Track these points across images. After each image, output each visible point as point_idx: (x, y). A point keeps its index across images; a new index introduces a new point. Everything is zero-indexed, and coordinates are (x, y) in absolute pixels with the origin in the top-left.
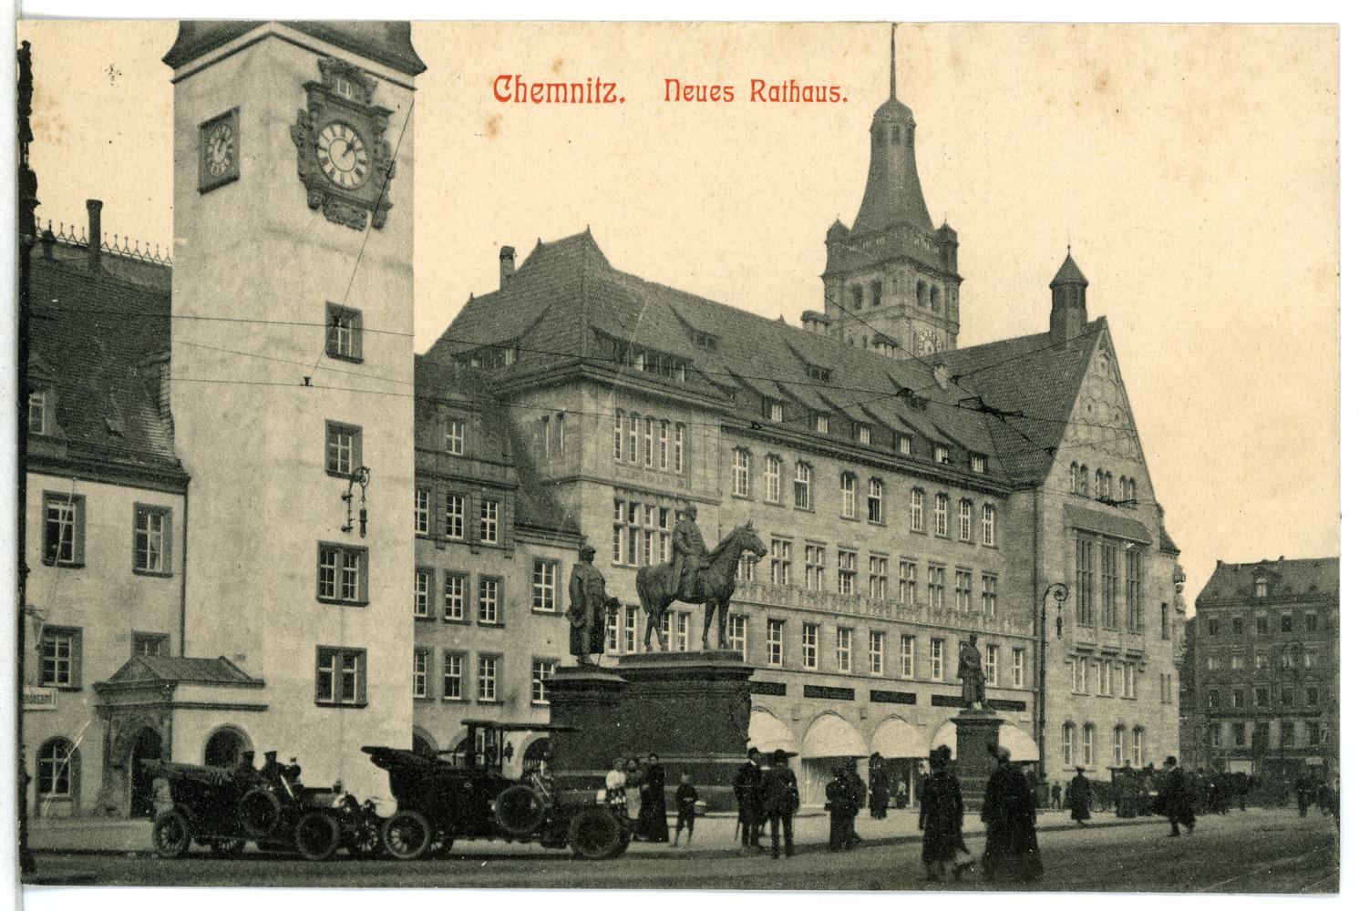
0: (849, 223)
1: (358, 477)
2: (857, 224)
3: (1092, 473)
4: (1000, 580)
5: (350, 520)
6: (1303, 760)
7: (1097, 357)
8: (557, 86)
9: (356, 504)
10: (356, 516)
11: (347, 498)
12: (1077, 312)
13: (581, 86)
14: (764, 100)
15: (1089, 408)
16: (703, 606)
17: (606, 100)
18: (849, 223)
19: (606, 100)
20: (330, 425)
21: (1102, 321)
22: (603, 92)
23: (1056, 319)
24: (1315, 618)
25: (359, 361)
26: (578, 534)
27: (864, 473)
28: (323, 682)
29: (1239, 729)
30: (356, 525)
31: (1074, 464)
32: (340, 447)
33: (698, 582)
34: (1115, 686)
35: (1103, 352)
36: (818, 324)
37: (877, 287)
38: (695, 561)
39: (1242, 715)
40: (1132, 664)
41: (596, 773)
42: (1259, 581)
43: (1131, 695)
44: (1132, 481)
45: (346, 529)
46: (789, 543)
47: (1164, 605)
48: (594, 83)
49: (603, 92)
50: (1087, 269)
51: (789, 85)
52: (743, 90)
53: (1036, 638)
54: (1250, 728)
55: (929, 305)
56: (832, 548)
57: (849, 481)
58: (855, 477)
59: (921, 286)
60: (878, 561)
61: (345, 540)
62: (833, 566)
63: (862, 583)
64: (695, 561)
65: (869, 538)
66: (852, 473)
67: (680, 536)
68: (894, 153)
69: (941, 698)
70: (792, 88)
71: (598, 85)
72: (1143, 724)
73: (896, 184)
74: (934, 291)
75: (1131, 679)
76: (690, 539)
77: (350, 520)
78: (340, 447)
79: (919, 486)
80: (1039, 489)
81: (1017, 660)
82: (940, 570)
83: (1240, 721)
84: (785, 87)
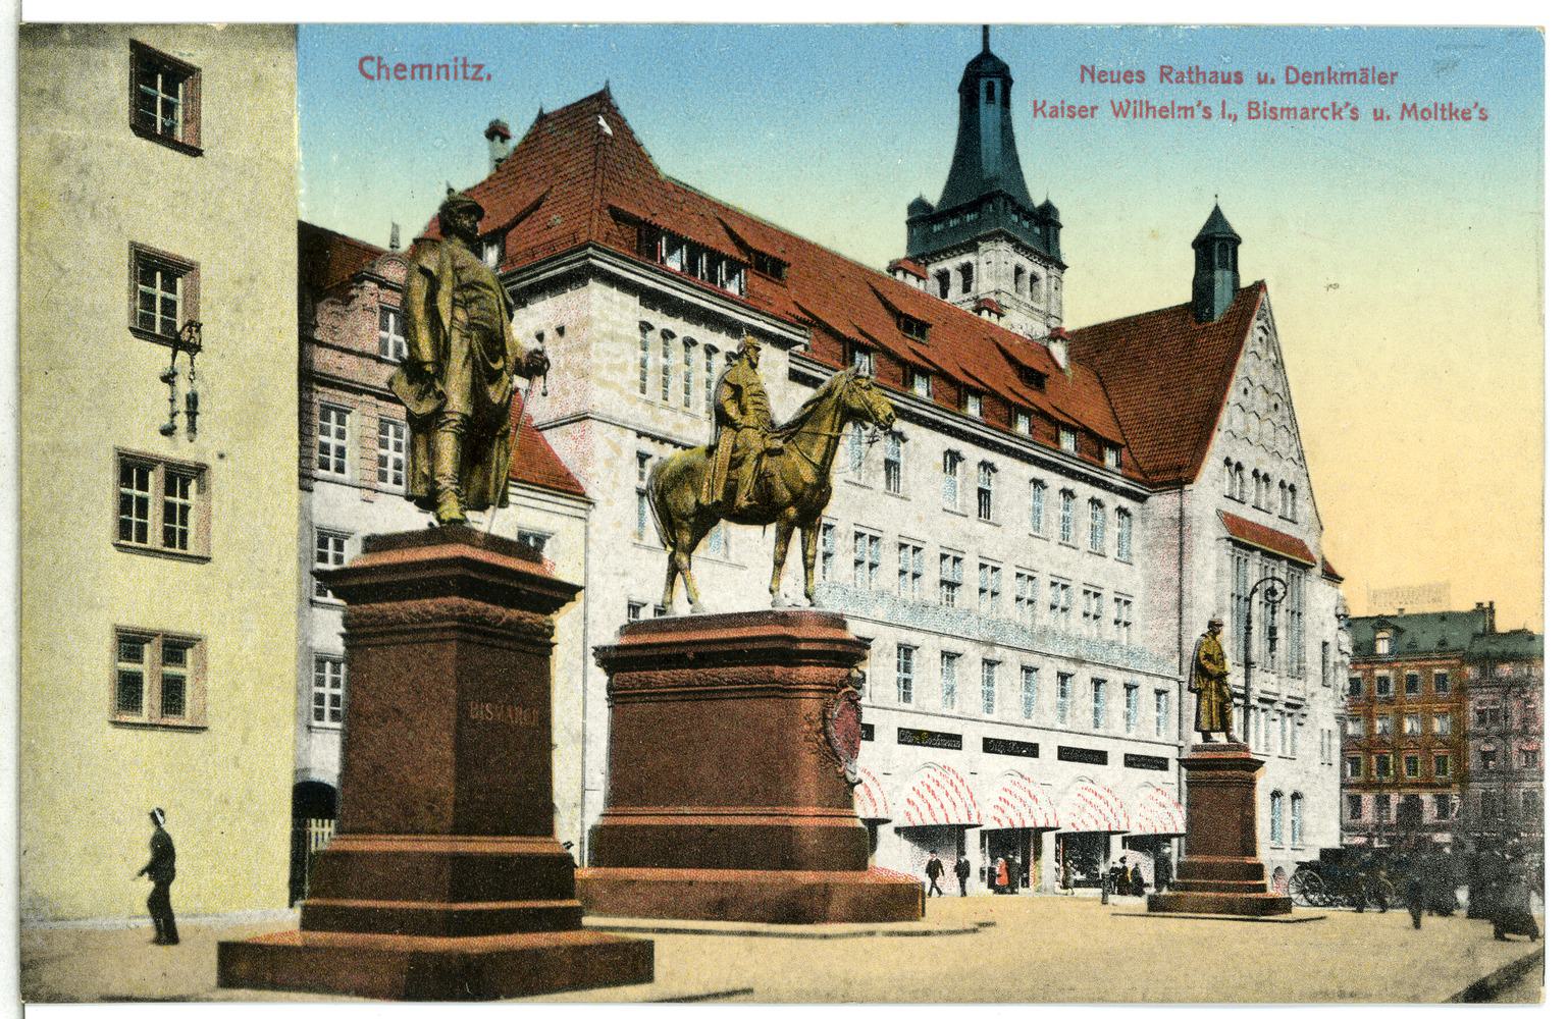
0: (934, 197)
1: (183, 342)
2: (943, 200)
3: (1248, 474)
4: (1136, 605)
5: (173, 415)
6: (1430, 837)
7: (1255, 333)
9: (183, 387)
10: (181, 406)
11: (169, 379)
12: (1228, 274)
13: (446, 66)
14: (1171, 82)
15: (1246, 392)
16: (772, 528)
18: (934, 197)
19: (474, 78)
20: (137, 253)
21: (1260, 286)
22: (471, 72)
23: (1203, 288)
24: (1444, 676)
25: (195, 152)
26: (583, 495)
27: (973, 454)
28: (128, 690)
29: (1382, 802)
30: (182, 421)
31: (1228, 462)
32: (159, 292)
33: (763, 479)
34: (1270, 741)
35: (1262, 323)
36: (908, 276)
37: (967, 271)
38: (754, 441)
39: (1417, 785)
40: (1290, 715)
41: (319, 937)
42: (1380, 635)
43: (1288, 754)
44: (1292, 488)
45: (168, 432)
46: (877, 539)
47: (1325, 644)
49: (471, 72)
50: (1237, 223)
53: (1182, 678)
54: (1395, 799)
55: (1028, 293)
56: (931, 552)
57: (953, 465)
58: (961, 459)
59: (1019, 271)
60: (989, 569)
61: (162, 448)
62: (932, 574)
63: (966, 597)
64: (754, 441)
65: (982, 540)
66: (957, 453)
67: (727, 392)
68: (988, 114)
69: (1069, 749)
70: (1198, 74)
71: (465, 65)
72: (1301, 789)
73: (991, 163)
74: (1034, 279)
75: (1288, 732)
76: (747, 400)
77: (173, 415)
78: (159, 292)
79: (1039, 477)
80: (1187, 487)
81: (1158, 705)
82: (1064, 587)
83: (1357, 792)
84: (1190, 72)
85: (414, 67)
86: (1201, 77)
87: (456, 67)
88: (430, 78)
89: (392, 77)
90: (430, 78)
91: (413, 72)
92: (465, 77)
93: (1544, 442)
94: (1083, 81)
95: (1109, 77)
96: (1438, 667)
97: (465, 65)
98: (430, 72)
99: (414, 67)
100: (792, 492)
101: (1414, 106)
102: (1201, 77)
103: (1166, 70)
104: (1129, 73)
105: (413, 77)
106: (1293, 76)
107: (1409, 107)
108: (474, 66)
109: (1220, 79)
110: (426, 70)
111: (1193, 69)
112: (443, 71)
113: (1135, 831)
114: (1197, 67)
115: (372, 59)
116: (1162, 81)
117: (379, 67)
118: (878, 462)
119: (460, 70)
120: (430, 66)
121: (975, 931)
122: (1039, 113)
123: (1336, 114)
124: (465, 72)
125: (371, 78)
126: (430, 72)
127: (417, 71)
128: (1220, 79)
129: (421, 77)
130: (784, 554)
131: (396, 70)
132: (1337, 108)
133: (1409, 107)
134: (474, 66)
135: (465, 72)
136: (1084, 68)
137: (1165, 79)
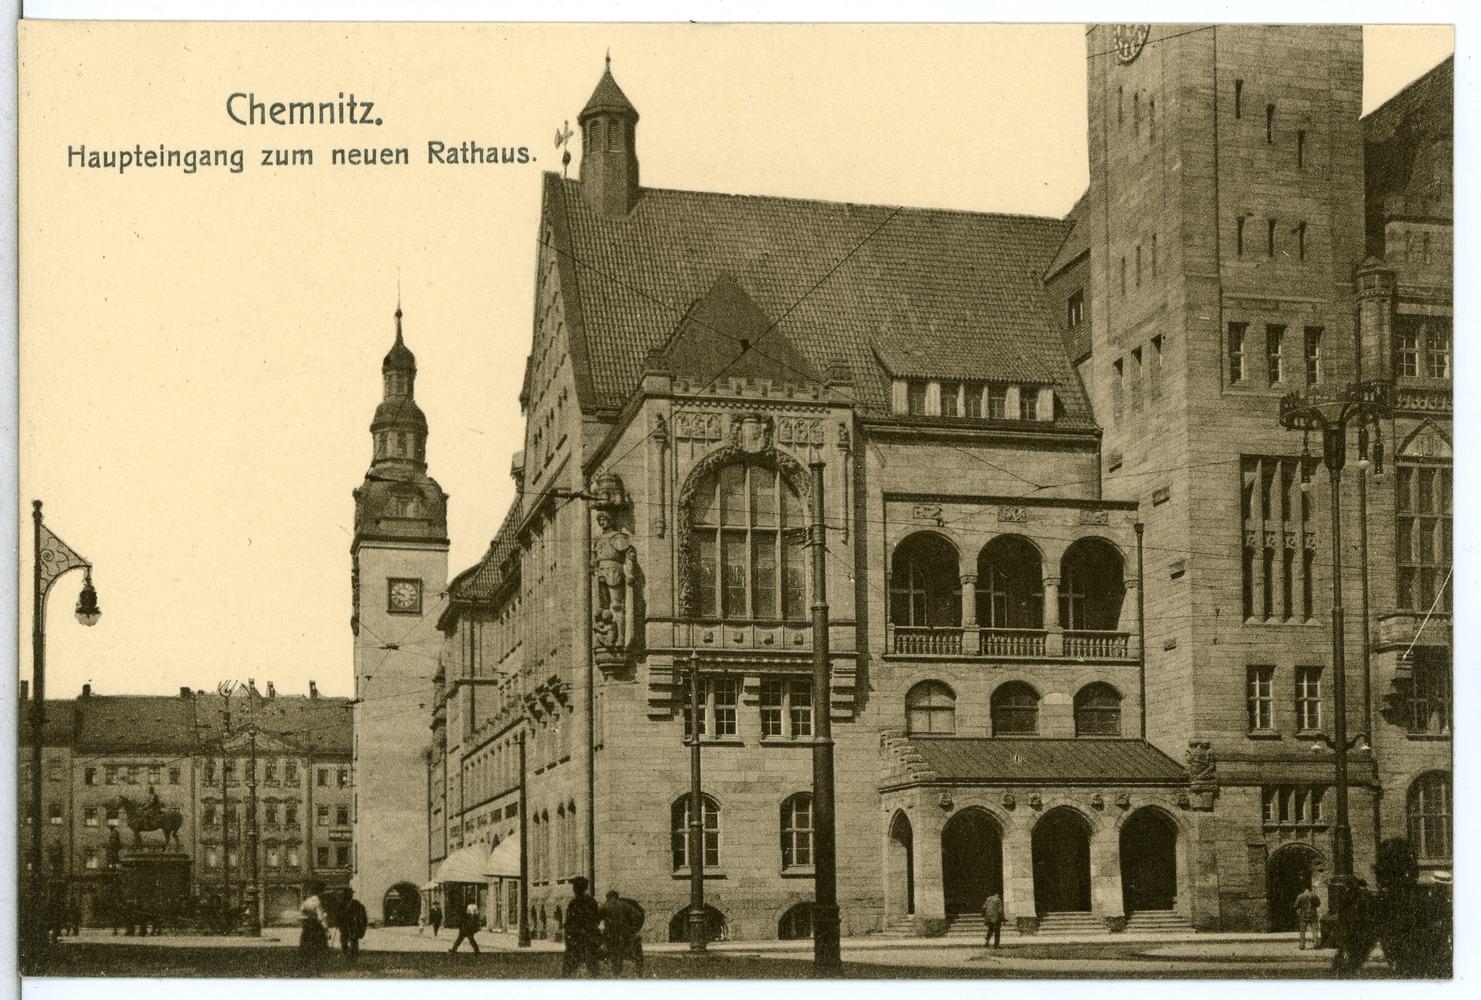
8: (302, 106)
13: (331, 106)
17: (363, 120)
19: (363, 120)
22: (359, 112)
48: (346, 100)
49: (359, 112)
51: (469, 146)
52: (419, 153)
70: (474, 151)
71: (352, 105)
84: (464, 150)
85: (292, 106)
86: (477, 155)
87: (341, 105)
88: (106, 154)
90: (106, 154)
93: (119, 21)
94: (334, 162)
95: (362, 158)
96: (750, 675)
98: (106, 159)
99: (292, 106)
102: (477, 155)
103: (436, 148)
104: (386, 152)
105: (397, 161)
106: (241, 107)
108: (362, 105)
109: (500, 158)
110: (307, 111)
111: (469, 146)
114: (473, 143)
116: (431, 161)
117: (253, 108)
119: (347, 110)
120: (311, 105)
121: (523, 493)
125: (244, 123)
126: (106, 159)
127: (297, 110)
128: (500, 158)
129: (302, 162)
130: (522, 487)
131: (350, 156)
134: (362, 105)
137: (434, 156)
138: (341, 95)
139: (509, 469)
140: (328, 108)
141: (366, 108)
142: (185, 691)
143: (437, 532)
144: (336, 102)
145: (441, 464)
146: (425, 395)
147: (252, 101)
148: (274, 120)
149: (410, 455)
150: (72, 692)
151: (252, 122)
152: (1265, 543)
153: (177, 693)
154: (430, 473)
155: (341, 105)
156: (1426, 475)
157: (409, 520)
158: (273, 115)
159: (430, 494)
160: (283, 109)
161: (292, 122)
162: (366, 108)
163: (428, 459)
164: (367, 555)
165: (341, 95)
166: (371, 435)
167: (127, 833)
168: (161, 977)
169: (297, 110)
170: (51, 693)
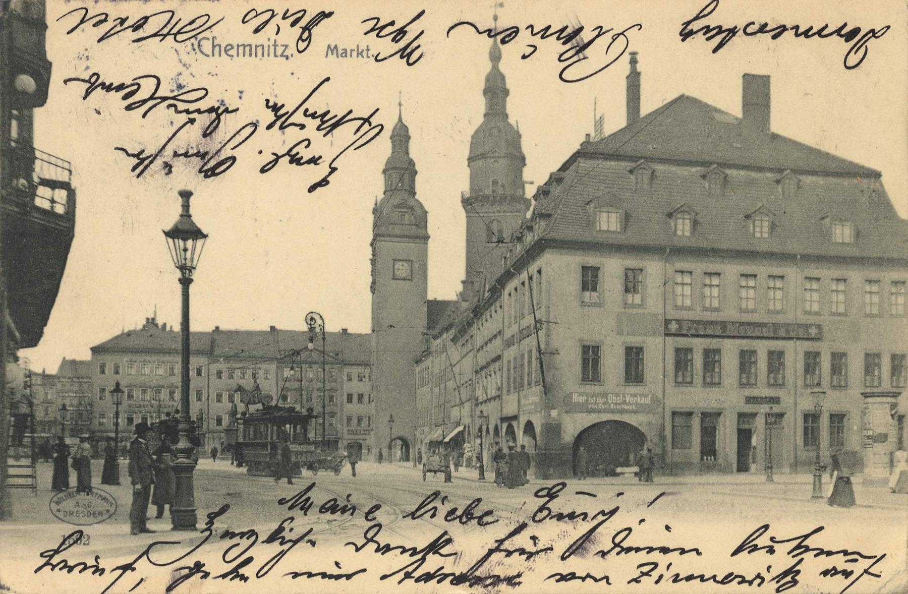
8: (244, 45)
13: (263, 46)
17: (282, 55)
19: (282, 55)
22: (280, 50)
48: (272, 42)
49: (280, 50)
71: (275, 45)
87: (269, 46)
88: (250, 55)
89: (223, 53)
91: (238, 49)
92: (276, 56)
97: (275, 45)
98: (250, 51)
99: (238, 46)
100: (833, 471)
101: (336, 47)
107: (332, 48)
108: (282, 45)
110: (247, 49)
112: (260, 50)
113: (424, 322)
115: (208, 39)
117: (214, 47)
118: (104, 112)
120: (250, 45)
122: (360, 56)
123: (360, 54)
124: (275, 52)
125: (208, 56)
126: (250, 51)
127: (241, 48)
132: (360, 51)
133: (332, 48)
134: (282, 45)
135: (275, 52)
136: (329, 46)
138: (269, 39)
139: (460, 199)
140: (261, 48)
141: (284, 48)
142: (273, 328)
143: (421, 232)
144: (266, 44)
145: (425, 191)
146: (414, 152)
147: (213, 42)
148: (228, 55)
149: (407, 187)
150: (209, 328)
151: (213, 55)
152: (409, 468)
153: (269, 329)
154: (417, 197)
155: (269, 46)
156: (637, 354)
157: (406, 225)
158: (226, 51)
159: (418, 211)
160: (232, 48)
161: (238, 55)
162: (284, 48)
163: (417, 190)
164: (381, 245)
165: (269, 39)
166: (383, 176)
167: (241, 407)
168: (851, 163)
169: (241, 48)
170: (194, 327)
